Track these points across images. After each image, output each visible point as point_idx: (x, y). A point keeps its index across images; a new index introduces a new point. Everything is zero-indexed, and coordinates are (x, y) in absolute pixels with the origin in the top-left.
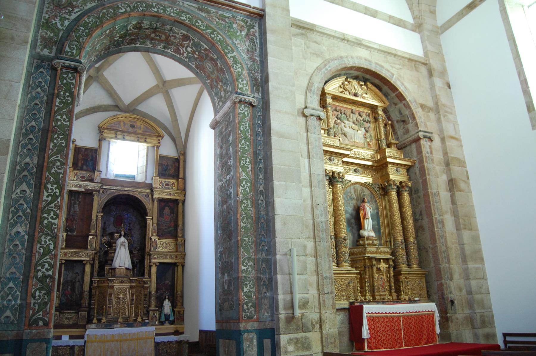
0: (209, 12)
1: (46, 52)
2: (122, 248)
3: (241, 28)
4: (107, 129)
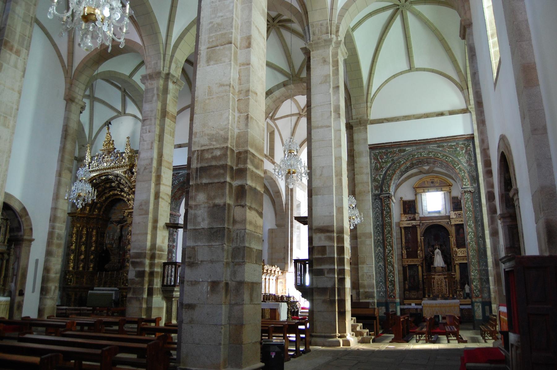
0: (443, 146)
1: (377, 192)
2: (438, 255)
3: (462, 149)
4: (418, 188)
